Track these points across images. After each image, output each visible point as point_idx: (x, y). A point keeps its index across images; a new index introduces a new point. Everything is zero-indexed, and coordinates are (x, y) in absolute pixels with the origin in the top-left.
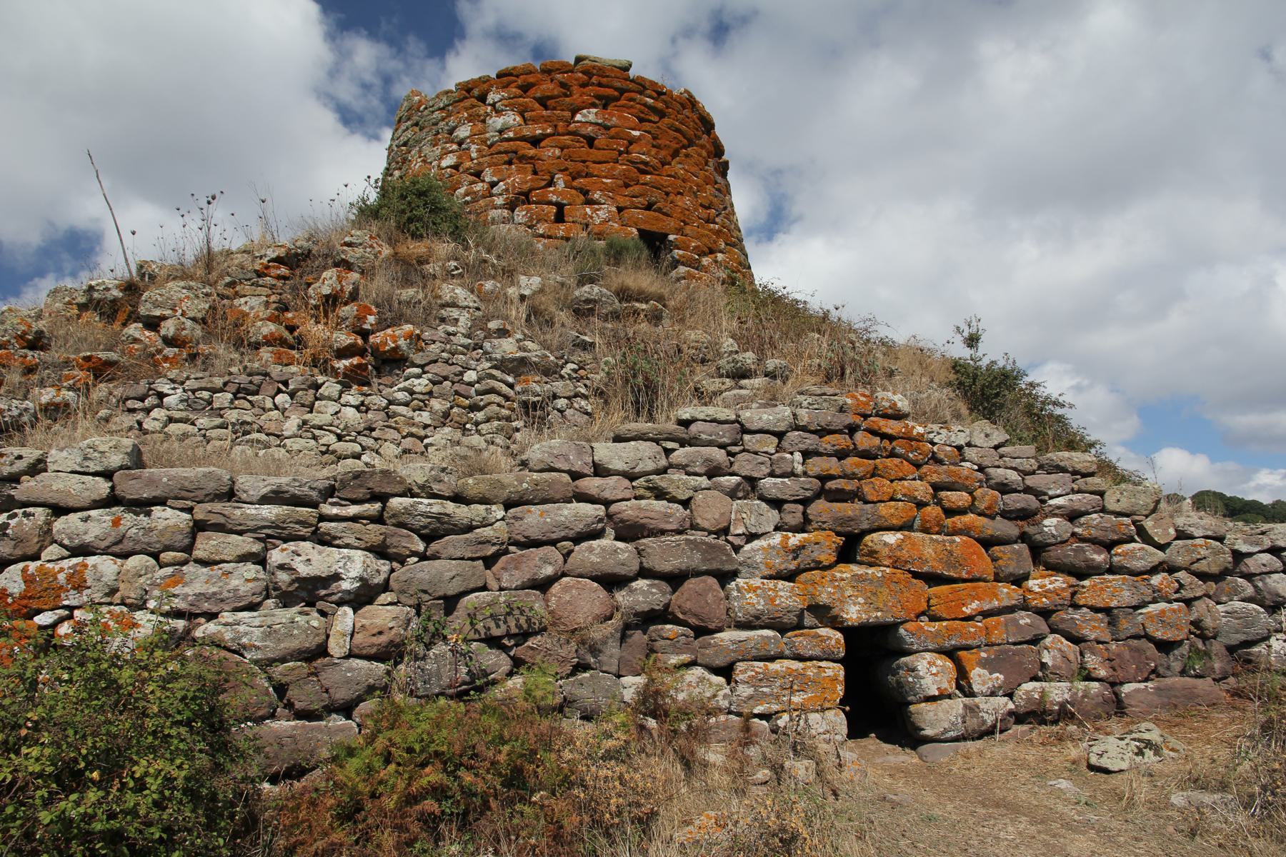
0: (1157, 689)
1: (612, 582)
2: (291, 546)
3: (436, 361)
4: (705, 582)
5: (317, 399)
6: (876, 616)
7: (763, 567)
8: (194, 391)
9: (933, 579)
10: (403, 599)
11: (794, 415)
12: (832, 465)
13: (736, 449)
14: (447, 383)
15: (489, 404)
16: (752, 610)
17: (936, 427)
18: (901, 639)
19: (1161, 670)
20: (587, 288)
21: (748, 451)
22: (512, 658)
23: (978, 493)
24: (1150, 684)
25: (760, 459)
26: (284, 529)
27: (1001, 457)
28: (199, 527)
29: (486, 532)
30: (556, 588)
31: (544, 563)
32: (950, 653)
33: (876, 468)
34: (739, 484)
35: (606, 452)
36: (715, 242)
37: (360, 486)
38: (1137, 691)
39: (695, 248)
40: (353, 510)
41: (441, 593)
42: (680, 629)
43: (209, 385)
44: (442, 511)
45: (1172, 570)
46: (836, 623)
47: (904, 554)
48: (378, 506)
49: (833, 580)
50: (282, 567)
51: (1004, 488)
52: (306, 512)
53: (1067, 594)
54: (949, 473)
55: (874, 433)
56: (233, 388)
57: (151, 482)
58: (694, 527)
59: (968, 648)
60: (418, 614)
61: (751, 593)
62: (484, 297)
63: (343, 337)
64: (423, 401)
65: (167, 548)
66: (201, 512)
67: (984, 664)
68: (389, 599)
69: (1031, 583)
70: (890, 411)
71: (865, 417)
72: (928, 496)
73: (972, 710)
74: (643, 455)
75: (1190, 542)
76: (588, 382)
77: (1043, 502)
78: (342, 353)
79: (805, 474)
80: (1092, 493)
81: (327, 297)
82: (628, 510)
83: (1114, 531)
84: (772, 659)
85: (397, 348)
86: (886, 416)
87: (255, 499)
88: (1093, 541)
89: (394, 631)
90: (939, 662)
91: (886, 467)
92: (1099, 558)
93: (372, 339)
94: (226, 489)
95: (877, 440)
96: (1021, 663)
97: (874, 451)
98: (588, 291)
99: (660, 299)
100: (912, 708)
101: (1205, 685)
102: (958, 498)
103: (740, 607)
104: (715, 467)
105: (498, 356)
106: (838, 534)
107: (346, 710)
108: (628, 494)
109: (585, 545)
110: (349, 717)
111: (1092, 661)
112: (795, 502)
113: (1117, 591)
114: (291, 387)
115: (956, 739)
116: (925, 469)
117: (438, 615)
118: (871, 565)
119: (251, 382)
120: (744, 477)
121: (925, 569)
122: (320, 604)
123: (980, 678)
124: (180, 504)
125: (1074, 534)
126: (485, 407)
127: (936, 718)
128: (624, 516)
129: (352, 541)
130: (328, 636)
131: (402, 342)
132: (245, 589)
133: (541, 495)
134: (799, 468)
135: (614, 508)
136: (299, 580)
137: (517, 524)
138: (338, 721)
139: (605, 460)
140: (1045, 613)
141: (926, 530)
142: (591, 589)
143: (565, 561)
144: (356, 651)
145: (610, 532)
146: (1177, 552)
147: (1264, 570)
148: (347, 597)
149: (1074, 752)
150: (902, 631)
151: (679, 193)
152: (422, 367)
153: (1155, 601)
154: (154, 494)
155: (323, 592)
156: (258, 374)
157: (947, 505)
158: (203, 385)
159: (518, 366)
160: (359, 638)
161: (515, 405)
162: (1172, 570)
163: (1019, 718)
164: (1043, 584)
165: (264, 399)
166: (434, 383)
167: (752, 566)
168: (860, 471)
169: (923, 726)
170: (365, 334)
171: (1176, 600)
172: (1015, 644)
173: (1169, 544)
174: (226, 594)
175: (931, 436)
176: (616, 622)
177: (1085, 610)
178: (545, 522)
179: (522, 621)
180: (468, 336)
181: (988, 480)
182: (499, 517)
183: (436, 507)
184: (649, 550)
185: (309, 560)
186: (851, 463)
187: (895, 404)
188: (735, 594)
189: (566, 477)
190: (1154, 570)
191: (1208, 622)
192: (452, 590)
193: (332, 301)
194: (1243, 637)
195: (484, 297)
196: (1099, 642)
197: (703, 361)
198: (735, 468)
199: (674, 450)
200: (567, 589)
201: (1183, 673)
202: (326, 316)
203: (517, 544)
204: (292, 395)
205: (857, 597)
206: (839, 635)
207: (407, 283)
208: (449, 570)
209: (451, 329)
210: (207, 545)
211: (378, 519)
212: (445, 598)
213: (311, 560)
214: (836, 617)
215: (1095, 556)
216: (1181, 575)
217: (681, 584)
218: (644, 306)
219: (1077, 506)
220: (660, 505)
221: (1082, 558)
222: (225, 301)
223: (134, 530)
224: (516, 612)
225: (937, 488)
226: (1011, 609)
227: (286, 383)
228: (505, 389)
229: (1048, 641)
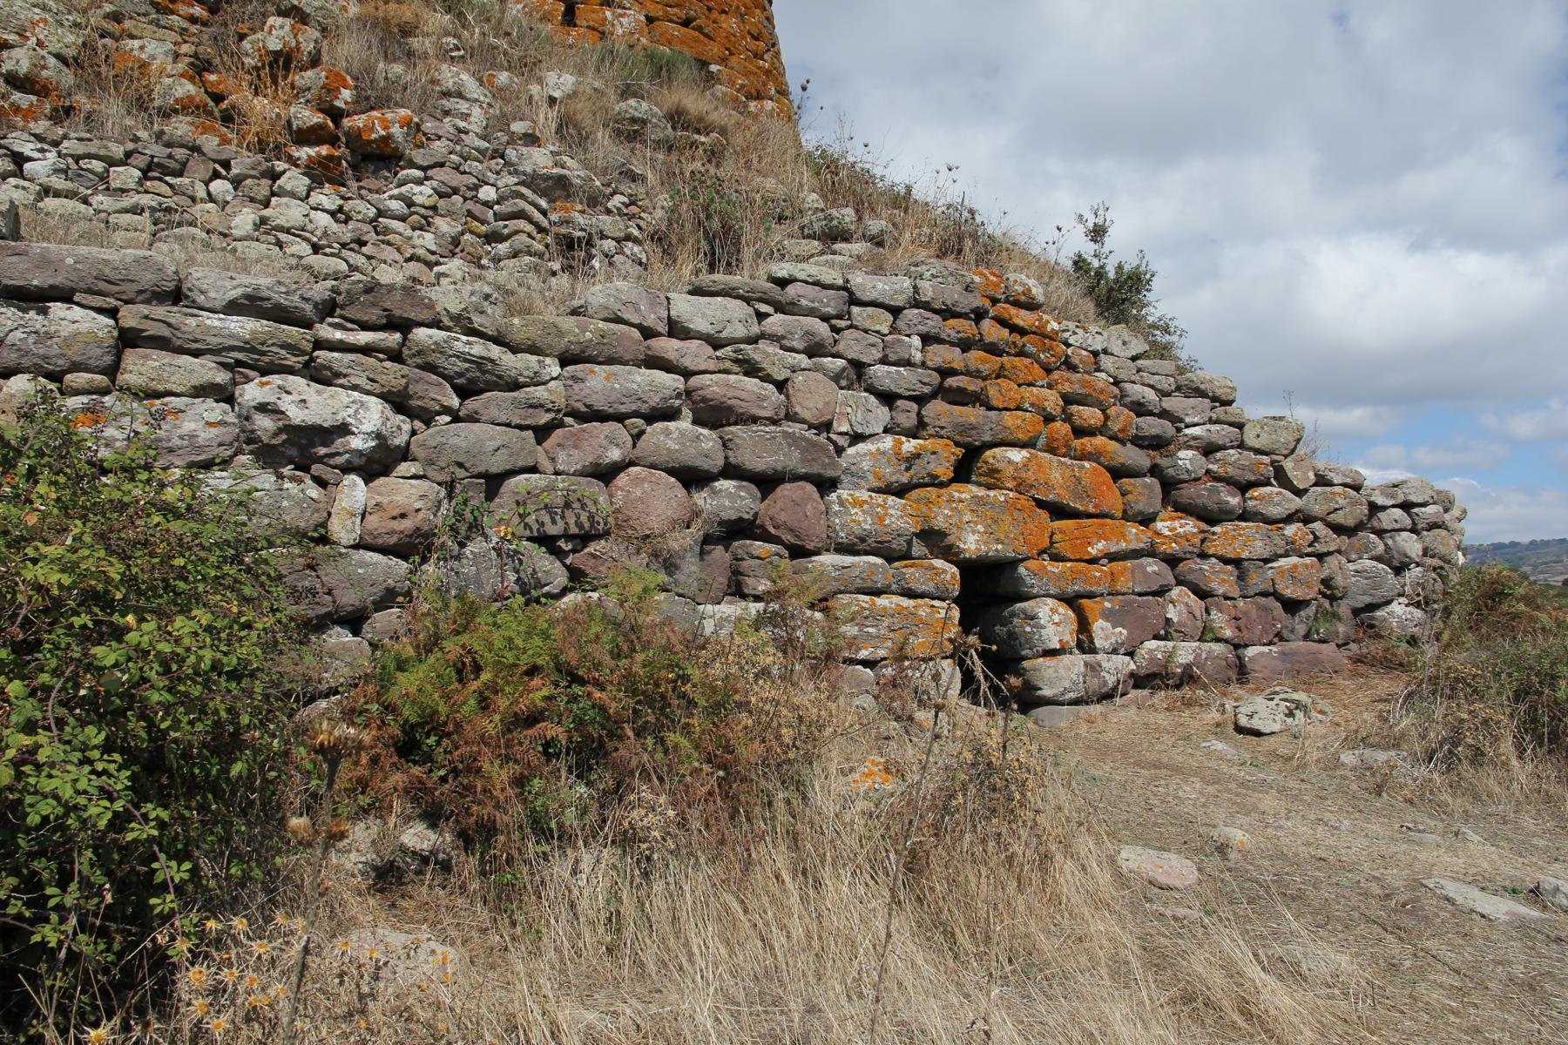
0: (1282, 653)
1: (692, 478)
2: (276, 379)
3: (442, 165)
4: (803, 488)
5: (273, 194)
6: (996, 549)
7: (870, 477)
8: (77, 159)
9: (1059, 511)
10: (430, 473)
11: (915, 287)
12: (953, 357)
13: (842, 323)
14: (457, 198)
15: (517, 232)
16: (857, 530)
17: (1071, 325)
18: (1020, 579)
19: (1285, 633)
20: (632, 102)
21: (856, 328)
22: (568, 567)
23: (1112, 411)
24: (1274, 648)
25: (872, 339)
26: (263, 353)
27: (1139, 370)
28: (128, 339)
29: (539, 393)
30: (622, 479)
31: (609, 443)
32: (1071, 601)
33: (1002, 367)
34: (844, 369)
35: (685, 307)
36: (765, 85)
37: (374, 305)
38: (1262, 654)
39: (743, 86)
40: (364, 337)
41: (482, 469)
42: (773, 548)
43: (102, 152)
44: (485, 354)
45: (1307, 520)
46: (949, 553)
47: (1030, 476)
48: (398, 336)
49: (951, 500)
50: (263, 408)
51: (1140, 409)
52: (295, 332)
53: (1197, 541)
54: (1084, 384)
55: (1003, 322)
56: (142, 161)
57: (45, 262)
58: (791, 417)
59: (1091, 596)
60: (450, 496)
61: (857, 509)
62: (499, 93)
63: (307, 113)
64: (425, 218)
65: (76, 367)
66: (130, 317)
67: (1108, 616)
68: (413, 471)
69: (1159, 525)
70: (1023, 298)
71: (995, 301)
72: (1059, 410)
73: (1093, 668)
74: (730, 316)
75: (1328, 489)
76: (642, 223)
77: (1179, 430)
78: (305, 136)
79: (923, 364)
80: (1231, 424)
81: (277, 54)
82: (713, 386)
83: (1252, 471)
84: (877, 593)
85: (387, 139)
86: (1017, 304)
87: (218, 305)
88: (1228, 481)
89: (421, 515)
90: (1061, 610)
91: (1015, 367)
92: (1234, 501)
93: (346, 122)
94: (171, 286)
95: (1006, 332)
96: (1145, 617)
97: (1002, 346)
98: (634, 107)
99: (723, 131)
100: (1025, 664)
101: (1328, 650)
102: (1089, 415)
103: (843, 526)
104: (817, 344)
105: (529, 170)
106: (957, 444)
107: (354, 621)
108: (711, 365)
109: (659, 425)
110: (356, 633)
111: (1218, 619)
112: (910, 398)
113: (1248, 540)
114: (235, 171)
115: (1075, 702)
116: (1056, 375)
117: (477, 499)
118: (989, 487)
119: (170, 156)
120: (849, 361)
121: (1051, 497)
122: (317, 469)
123: (1104, 633)
124: (97, 301)
125: (1208, 472)
126: (509, 236)
127: (1058, 675)
128: (707, 393)
129: (361, 381)
130: (329, 514)
131: (396, 130)
132: (206, 435)
133: (607, 351)
134: (918, 357)
135: (695, 381)
136: (291, 429)
137: (576, 386)
138: (339, 637)
139: (685, 317)
140: (1172, 561)
141: (1052, 450)
142: (667, 484)
143: (634, 446)
144: (369, 539)
145: (687, 413)
146: (1315, 502)
147: (1397, 526)
148: (357, 461)
149: (1213, 715)
150: (1022, 570)
151: (724, 12)
152: (424, 169)
153: (1286, 555)
154: (51, 282)
155: (322, 451)
156: (182, 146)
157: (1078, 422)
158: (93, 150)
159: (555, 188)
160: (372, 520)
161: (549, 239)
162: (1307, 520)
163: (1140, 681)
164: (1174, 528)
165: (192, 182)
166: (441, 195)
167: (857, 476)
168: (985, 368)
169: (1040, 684)
170: (336, 115)
171: (1308, 555)
172: (1140, 594)
173: (1306, 491)
174: (176, 442)
175: (1066, 335)
176: (695, 532)
177: (1214, 560)
178: (613, 389)
179: (584, 518)
180: (484, 138)
181: (1122, 397)
182: (554, 374)
183: (478, 348)
184: (737, 441)
185: (304, 401)
186: (975, 355)
187: (1029, 290)
188: (837, 508)
189: (636, 334)
190: (1289, 519)
191: (1339, 581)
192: (496, 465)
193: (282, 62)
194: (1368, 599)
195: (499, 93)
196: (1227, 598)
197: (781, 219)
198: (840, 347)
199: (768, 315)
200: (637, 481)
201: (1307, 637)
202: (275, 82)
203: (574, 414)
204: (237, 182)
205: (976, 523)
206: (955, 569)
207: (389, 58)
208: (492, 438)
209: (462, 124)
210: (140, 367)
211: (396, 356)
212: (485, 476)
213: (307, 403)
214: (951, 547)
215: (1229, 499)
216: (1317, 526)
217: (772, 490)
218: (703, 139)
219: (1215, 438)
220: (752, 384)
221: (1215, 499)
222: (107, 41)
223: (18, 334)
224: (576, 505)
225: (1068, 400)
226: (1136, 554)
227: (226, 165)
228: (537, 216)
229: (1175, 592)
